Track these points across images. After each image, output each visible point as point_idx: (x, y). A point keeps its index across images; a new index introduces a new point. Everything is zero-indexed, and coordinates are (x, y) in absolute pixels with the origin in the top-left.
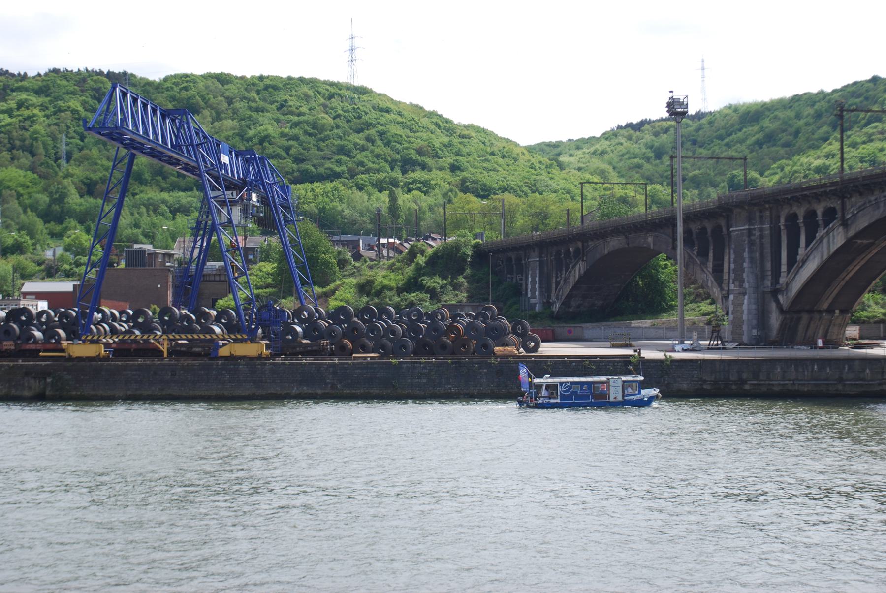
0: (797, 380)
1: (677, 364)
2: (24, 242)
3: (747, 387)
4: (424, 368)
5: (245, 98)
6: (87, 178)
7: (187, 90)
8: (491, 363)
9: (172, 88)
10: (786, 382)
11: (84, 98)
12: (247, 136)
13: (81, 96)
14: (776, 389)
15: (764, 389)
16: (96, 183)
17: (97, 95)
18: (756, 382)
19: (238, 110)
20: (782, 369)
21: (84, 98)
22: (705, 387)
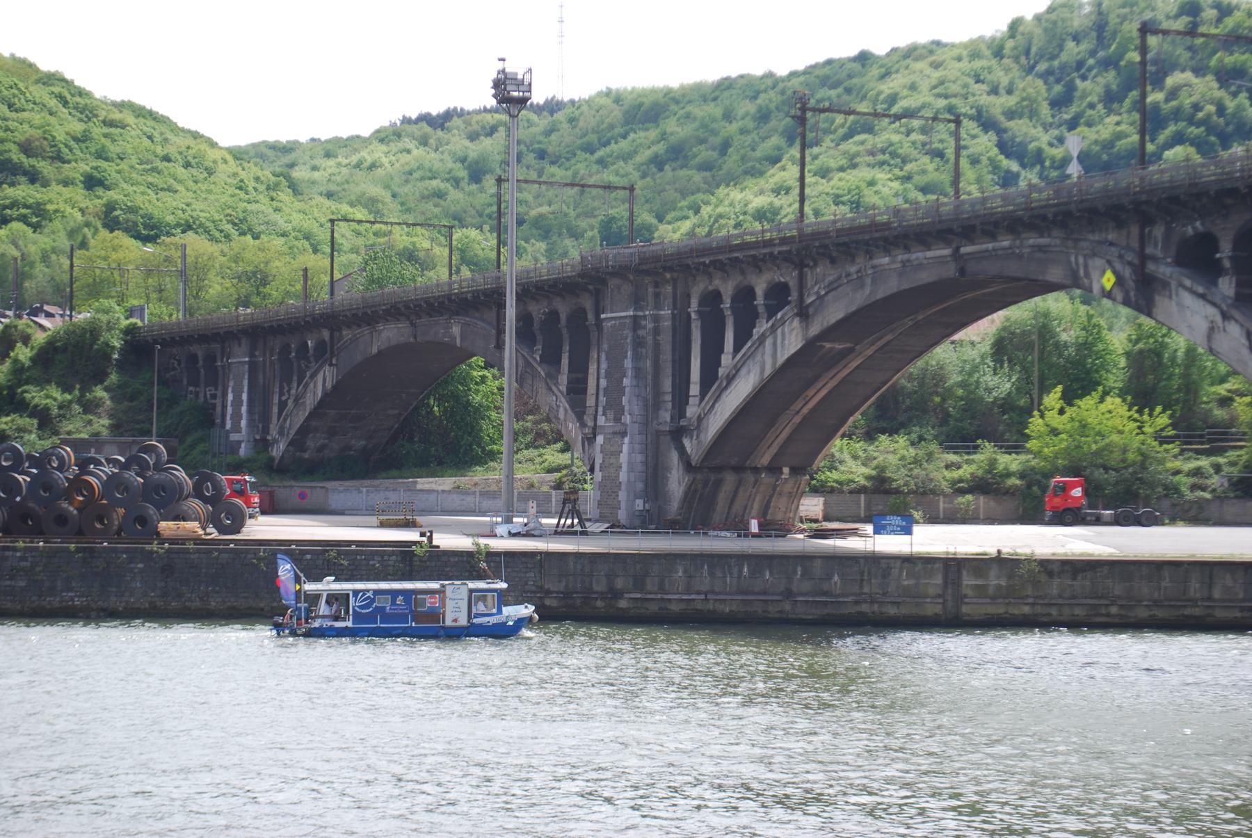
0: (712, 592)
3: (623, 604)
14: (675, 607)
20: (685, 571)
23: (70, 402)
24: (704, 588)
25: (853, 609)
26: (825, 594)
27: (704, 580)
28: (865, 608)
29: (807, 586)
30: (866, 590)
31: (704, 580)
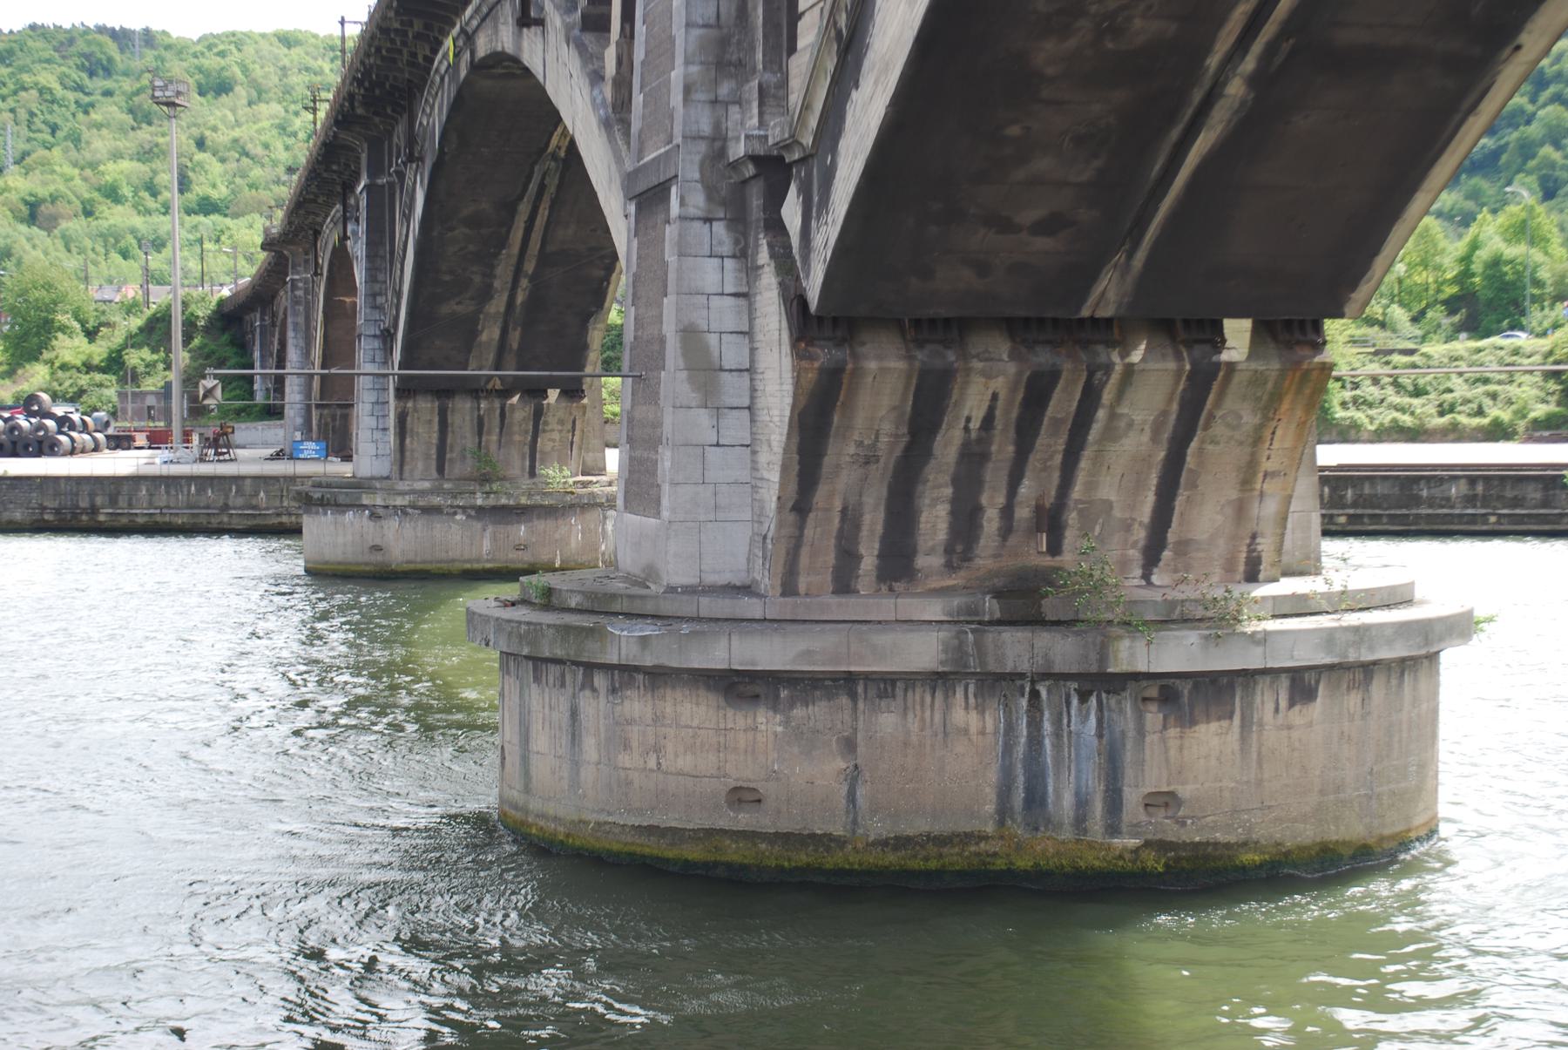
0: (168, 507)
3: (102, 518)
5: (307, 69)
6: (31, 195)
7: (224, 57)
9: (202, 54)
10: (152, 511)
11: (64, 69)
12: (290, 129)
13: (60, 65)
14: (140, 520)
15: (124, 520)
16: (44, 201)
17: (87, 64)
18: (110, 511)
19: (293, 88)
20: (147, 490)
21: (64, 69)
22: (46, 517)
23: (156, 361)
24: (162, 504)
25: (276, 520)
26: (254, 508)
27: (162, 499)
28: (285, 519)
29: (240, 501)
30: (285, 504)
31: (162, 499)
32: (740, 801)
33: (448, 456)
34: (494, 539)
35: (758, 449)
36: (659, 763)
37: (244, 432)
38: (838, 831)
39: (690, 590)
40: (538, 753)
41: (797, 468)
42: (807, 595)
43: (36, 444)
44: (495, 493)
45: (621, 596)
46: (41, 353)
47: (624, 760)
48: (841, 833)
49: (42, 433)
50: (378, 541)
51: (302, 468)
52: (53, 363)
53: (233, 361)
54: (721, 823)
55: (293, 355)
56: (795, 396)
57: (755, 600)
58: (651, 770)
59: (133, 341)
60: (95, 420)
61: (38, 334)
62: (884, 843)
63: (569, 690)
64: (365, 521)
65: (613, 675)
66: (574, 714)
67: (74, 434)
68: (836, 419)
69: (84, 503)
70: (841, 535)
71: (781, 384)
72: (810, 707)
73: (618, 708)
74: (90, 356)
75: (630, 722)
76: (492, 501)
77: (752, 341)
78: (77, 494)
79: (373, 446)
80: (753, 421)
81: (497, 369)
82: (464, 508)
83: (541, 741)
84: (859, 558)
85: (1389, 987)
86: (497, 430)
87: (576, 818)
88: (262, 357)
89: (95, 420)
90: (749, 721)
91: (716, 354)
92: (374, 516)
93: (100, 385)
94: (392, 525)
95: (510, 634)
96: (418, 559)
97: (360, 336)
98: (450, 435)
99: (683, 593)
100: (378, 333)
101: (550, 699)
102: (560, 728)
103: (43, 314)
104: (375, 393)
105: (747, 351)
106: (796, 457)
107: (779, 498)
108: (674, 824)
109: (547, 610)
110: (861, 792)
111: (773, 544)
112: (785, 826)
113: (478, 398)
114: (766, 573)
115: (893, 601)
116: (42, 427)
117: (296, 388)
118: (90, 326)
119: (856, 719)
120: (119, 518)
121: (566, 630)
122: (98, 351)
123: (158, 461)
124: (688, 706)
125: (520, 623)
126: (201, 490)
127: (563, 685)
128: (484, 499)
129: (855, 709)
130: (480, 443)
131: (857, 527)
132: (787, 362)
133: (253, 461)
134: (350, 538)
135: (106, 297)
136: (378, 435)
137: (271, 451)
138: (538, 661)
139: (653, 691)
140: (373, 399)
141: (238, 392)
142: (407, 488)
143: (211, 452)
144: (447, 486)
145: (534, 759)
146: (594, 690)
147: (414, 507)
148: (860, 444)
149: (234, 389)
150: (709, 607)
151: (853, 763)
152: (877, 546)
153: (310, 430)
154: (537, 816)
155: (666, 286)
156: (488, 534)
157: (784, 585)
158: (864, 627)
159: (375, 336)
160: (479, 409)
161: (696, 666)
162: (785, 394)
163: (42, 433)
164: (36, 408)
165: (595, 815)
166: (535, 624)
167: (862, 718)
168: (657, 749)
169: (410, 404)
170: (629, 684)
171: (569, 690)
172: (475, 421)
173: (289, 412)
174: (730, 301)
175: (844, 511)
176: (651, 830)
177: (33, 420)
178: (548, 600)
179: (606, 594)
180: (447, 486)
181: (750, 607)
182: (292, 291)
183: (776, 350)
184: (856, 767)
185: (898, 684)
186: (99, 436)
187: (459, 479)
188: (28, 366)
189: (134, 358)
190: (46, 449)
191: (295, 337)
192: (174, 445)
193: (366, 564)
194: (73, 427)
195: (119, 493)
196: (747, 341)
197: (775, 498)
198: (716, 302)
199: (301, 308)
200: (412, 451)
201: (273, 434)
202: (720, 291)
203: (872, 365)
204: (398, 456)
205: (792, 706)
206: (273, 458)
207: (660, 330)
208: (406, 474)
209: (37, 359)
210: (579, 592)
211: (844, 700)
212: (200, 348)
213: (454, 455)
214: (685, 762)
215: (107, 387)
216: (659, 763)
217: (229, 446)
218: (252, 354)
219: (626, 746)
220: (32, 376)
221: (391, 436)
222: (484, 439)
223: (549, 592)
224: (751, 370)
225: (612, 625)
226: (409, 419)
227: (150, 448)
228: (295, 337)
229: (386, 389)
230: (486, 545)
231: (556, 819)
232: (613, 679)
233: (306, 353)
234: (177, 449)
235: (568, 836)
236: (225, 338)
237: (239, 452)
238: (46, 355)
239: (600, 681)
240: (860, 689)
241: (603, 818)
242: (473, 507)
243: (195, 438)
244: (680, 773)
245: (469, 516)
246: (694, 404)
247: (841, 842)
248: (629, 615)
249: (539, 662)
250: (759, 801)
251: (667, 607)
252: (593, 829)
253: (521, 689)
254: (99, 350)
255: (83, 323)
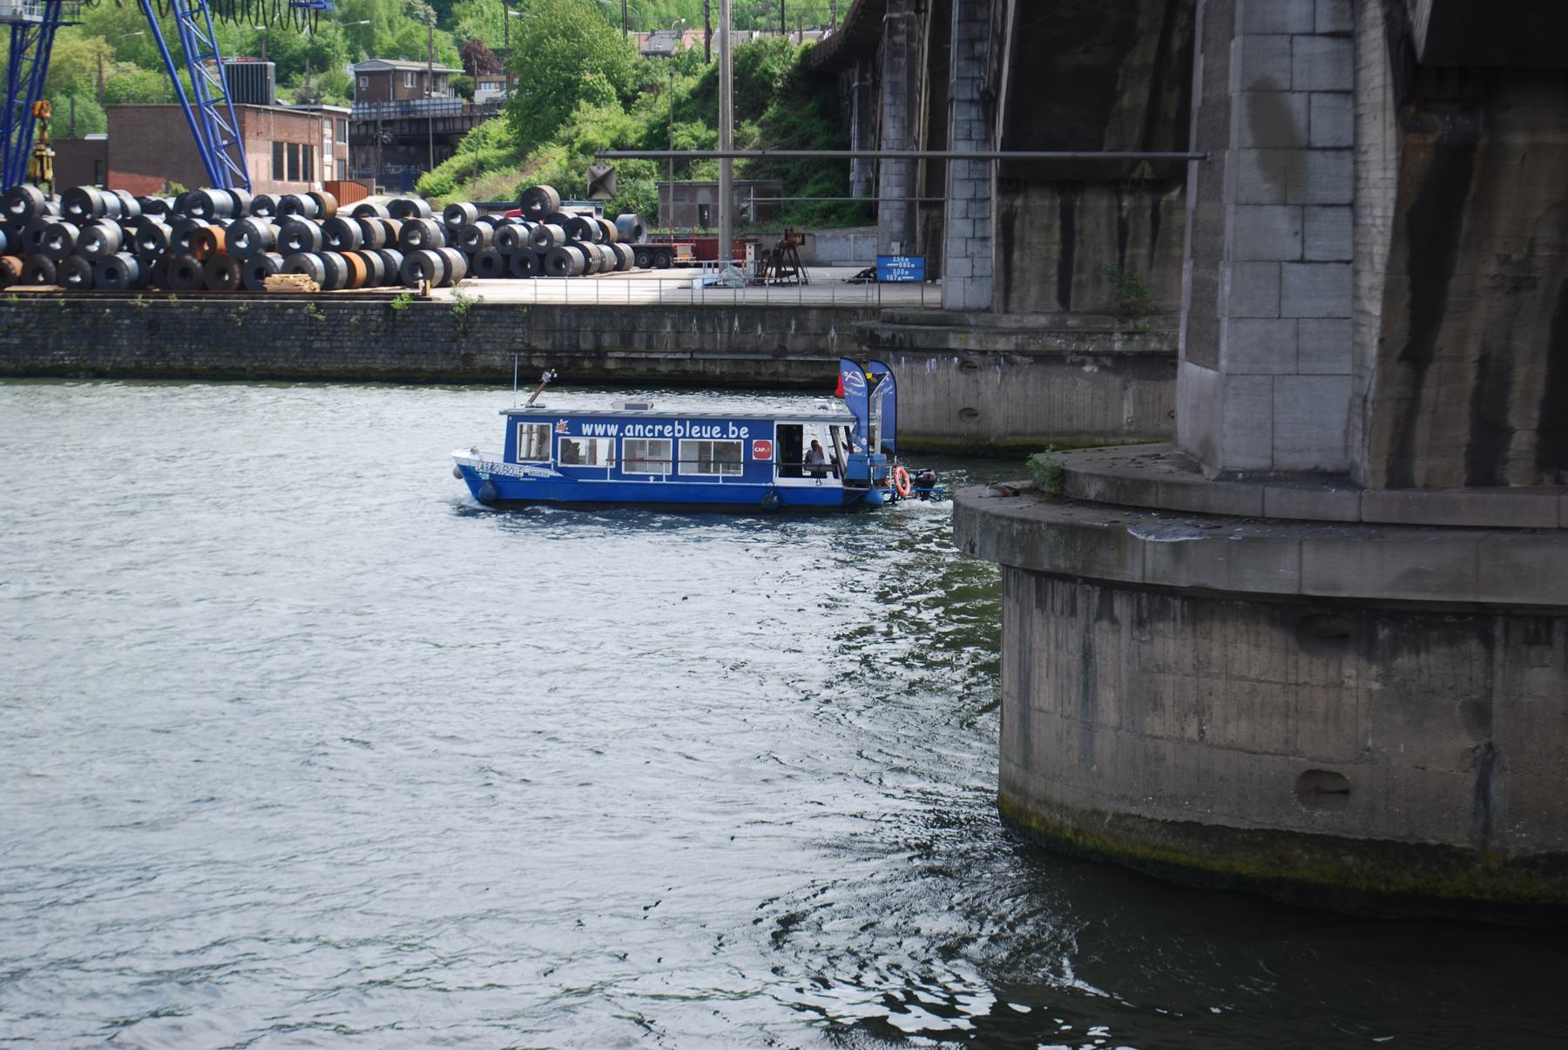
0: (701, 350)
1: (484, 313)
2: (328, 46)
3: (610, 365)
4: (17, 314)
8: (136, 306)
10: (679, 356)
15: (642, 369)
18: (623, 355)
20: (673, 326)
24: (693, 346)
26: (821, 352)
29: (801, 343)
31: (693, 338)
32: (1319, 792)
33: (1075, 278)
34: (1139, 401)
35: (1361, 267)
36: (1202, 731)
37: (827, 242)
38: (1460, 840)
39: (1256, 477)
40: (1040, 710)
41: (1408, 295)
42: (1427, 487)
43: (536, 259)
44: (1141, 333)
45: (1156, 483)
46: (557, 130)
47: (1155, 724)
48: (1466, 845)
49: (544, 244)
50: (971, 403)
51: (891, 296)
52: (572, 143)
53: (820, 140)
54: (1290, 823)
55: (891, 130)
56: (1401, 186)
57: (1345, 494)
58: (1191, 741)
59: (682, 111)
60: (621, 225)
61: (556, 102)
62: (1528, 863)
63: (1081, 619)
64: (953, 372)
65: (1139, 599)
66: (1087, 654)
67: (589, 245)
68: (1465, 223)
69: (586, 344)
70: (1478, 399)
71: (1385, 169)
72: (1423, 655)
73: (1146, 648)
74: (623, 133)
75: (1163, 669)
76: (1136, 345)
77: (1356, 105)
78: (577, 331)
79: (966, 264)
80: (1355, 224)
81: (1145, 149)
82: (1095, 356)
83: (1044, 695)
84: (1509, 433)
85: (945, 1003)
86: (1148, 240)
87: (1088, 807)
88: (862, 134)
89: (621, 225)
90: (1332, 673)
91: (1302, 124)
92: (966, 366)
93: (635, 175)
94: (991, 380)
95: (999, 535)
96: (1029, 430)
97: (952, 100)
98: (1077, 248)
99: (1244, 481)
100: (976, 96)
101: (1057, 631)
102: (1069, 675)
103: (565, 75)
104: (971, 185)
105: (1349, 119)
106: (1405, 278)
107: (1381, 341)
108: (1221, 821)
109: (1058, 503)
110: (1497, 785)
111: (1375, 410)
112: (1382, 830)
113: (1118, 194)
114: (1366, 454)
115: (1554, 498)
116: (545, 234)
117: (894, 179)
118: (628, 90)
119: (1491, 675)
120: (635, 365)
121: (1072, 531)
122: (634, 125)
123: (698, 284)
124: (1244, 647)
125: (1011, 519)
126: (747, 326)
127: (1073, 613)
128: (1125, 342)
129: (1490, 660)
130: (1122, 259)
131: (1505, 385)
132: (1391, 134)
133: (832, 284)
134: (931, 396)
135: (662, 48)
136: (974, 247)
137: (854, 271)
138: (1045, 578)
139: (1195, 624)
140: (968, 194)
141: (827, 184)
142: (1015, 325)
143: (772, 271)
144: (1072, 322)
145: (1036, 717)
146: (1114, 621)
147: (1023, 353)
148: (1504, 260)
149: (821, 181)
150: (1277, 501)
151: (1486, 740)
152: (1536, 414)
153: (913, 240)
154: (1039, 802)
155: (1232, 24)
156: (1130, 393)
157: (1390, 471)
158: (1506, 537)
159: (971, 102)
160: (1120, 208)
161: (1251, 588)
162: (1389, 182)
163: (544, 244)
164: (538, 207)
165: (1113, 804)
166: (1031, 522)
167: (1500, 674)
168: (1200, 710)
169: (1019, 202)
170: (1161, 613)
171: (1081, 619)
172: (1115, 226)
173: (884, 214)
174: (1325, 45)
175: (1483, 361)
176: (1190, 829)
177: (533, 225)
178: (1060, 488)
179: (1135, 480)
180: (1072, 322)
181: (1339, 503)
182: (890, 36)
183: (1380, 118)
184: (1490, 746)
185: (1558, 624)
186: (625, 248)
187: (1089, 313)
188: (541, 148)
189: (685, 136)
190: (550, 267)
191: (893, 104)
192: (720, 262)
193: (954, 435)
194: (588, 235)
195: (634, 330)
196: (1350, 105)
197: (1376, 341)
198: (1303, 46)
199: (903, 61)
200: (1023, 270)
201: (860, 244)
202: (1309, 29)
203: (1518, 140)
204: (1002, 277)
205: (1395, 652)
206: (858, 281)
207: (1226, 88)
208: (1014, 305)
209: (550, 137)
210: (1101, 477)
211: (1474, 647)
212: (776, 121)
213: (1084, 277)
214: (1238, 731)
215: (645, 177)
216: (1202, 731)
217: (796, 263)
218: (849, 129)
219: (1157, 704)
220: (546, 161)
221: (992, 250)
222: (1128, 252)
223: (1061, 476)
224: (1354, 149)
225: (1135, 525)
226: (1017, 223)
227: (698, 266)
228: (893, 104)
229: (986, 180)
230: (1128, 410)
231: (1062, 807)
232: (1139, 604)
233: (908, 128)
234: (724, 267)
235: (1077, 832)
236: (812, 105)
237: (813, 272)
238: (564, 132)
239: (1122, 607)
240: (1498, 630)
241: (1124, 808)
242: (1109, 354)
243: (750, 251)
244: (1231, 747)
245: (1103, 368)
246: (1266, 199)
247: (1463, 858)
248: (1166, 513)
249: (1045, 578)
250: (1346, 792)
251: (1219, 501)
252: (1110, 824)
253: (1021, 617)
254: (635, 124)
255: (619, 85)
